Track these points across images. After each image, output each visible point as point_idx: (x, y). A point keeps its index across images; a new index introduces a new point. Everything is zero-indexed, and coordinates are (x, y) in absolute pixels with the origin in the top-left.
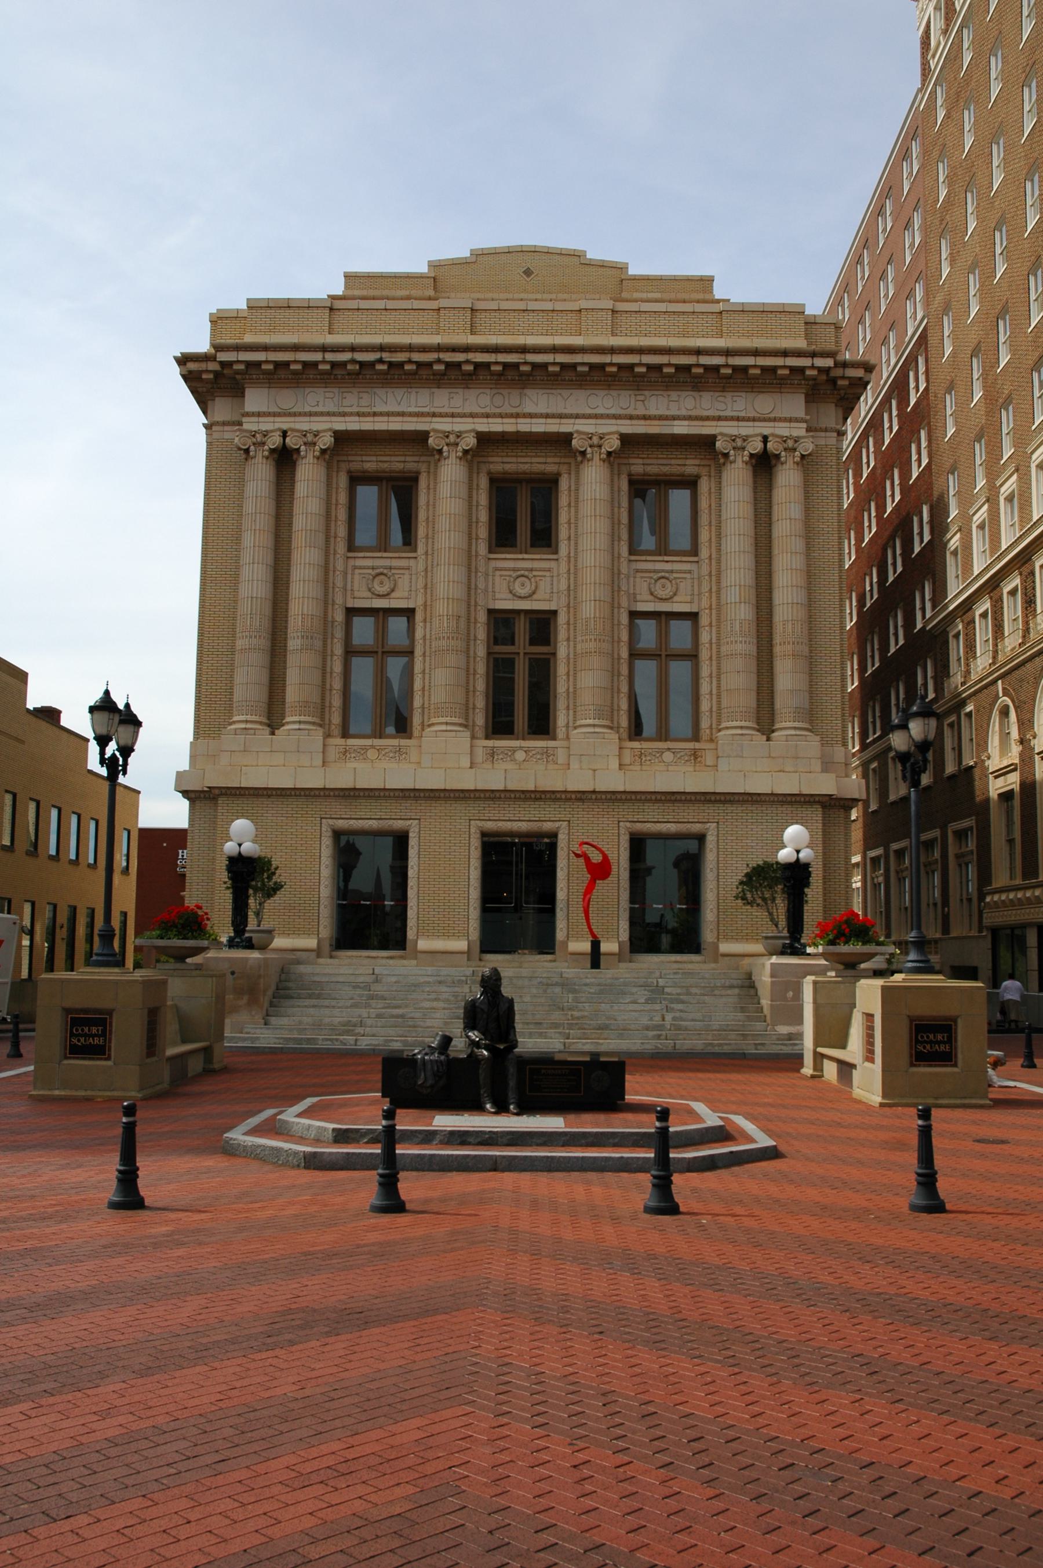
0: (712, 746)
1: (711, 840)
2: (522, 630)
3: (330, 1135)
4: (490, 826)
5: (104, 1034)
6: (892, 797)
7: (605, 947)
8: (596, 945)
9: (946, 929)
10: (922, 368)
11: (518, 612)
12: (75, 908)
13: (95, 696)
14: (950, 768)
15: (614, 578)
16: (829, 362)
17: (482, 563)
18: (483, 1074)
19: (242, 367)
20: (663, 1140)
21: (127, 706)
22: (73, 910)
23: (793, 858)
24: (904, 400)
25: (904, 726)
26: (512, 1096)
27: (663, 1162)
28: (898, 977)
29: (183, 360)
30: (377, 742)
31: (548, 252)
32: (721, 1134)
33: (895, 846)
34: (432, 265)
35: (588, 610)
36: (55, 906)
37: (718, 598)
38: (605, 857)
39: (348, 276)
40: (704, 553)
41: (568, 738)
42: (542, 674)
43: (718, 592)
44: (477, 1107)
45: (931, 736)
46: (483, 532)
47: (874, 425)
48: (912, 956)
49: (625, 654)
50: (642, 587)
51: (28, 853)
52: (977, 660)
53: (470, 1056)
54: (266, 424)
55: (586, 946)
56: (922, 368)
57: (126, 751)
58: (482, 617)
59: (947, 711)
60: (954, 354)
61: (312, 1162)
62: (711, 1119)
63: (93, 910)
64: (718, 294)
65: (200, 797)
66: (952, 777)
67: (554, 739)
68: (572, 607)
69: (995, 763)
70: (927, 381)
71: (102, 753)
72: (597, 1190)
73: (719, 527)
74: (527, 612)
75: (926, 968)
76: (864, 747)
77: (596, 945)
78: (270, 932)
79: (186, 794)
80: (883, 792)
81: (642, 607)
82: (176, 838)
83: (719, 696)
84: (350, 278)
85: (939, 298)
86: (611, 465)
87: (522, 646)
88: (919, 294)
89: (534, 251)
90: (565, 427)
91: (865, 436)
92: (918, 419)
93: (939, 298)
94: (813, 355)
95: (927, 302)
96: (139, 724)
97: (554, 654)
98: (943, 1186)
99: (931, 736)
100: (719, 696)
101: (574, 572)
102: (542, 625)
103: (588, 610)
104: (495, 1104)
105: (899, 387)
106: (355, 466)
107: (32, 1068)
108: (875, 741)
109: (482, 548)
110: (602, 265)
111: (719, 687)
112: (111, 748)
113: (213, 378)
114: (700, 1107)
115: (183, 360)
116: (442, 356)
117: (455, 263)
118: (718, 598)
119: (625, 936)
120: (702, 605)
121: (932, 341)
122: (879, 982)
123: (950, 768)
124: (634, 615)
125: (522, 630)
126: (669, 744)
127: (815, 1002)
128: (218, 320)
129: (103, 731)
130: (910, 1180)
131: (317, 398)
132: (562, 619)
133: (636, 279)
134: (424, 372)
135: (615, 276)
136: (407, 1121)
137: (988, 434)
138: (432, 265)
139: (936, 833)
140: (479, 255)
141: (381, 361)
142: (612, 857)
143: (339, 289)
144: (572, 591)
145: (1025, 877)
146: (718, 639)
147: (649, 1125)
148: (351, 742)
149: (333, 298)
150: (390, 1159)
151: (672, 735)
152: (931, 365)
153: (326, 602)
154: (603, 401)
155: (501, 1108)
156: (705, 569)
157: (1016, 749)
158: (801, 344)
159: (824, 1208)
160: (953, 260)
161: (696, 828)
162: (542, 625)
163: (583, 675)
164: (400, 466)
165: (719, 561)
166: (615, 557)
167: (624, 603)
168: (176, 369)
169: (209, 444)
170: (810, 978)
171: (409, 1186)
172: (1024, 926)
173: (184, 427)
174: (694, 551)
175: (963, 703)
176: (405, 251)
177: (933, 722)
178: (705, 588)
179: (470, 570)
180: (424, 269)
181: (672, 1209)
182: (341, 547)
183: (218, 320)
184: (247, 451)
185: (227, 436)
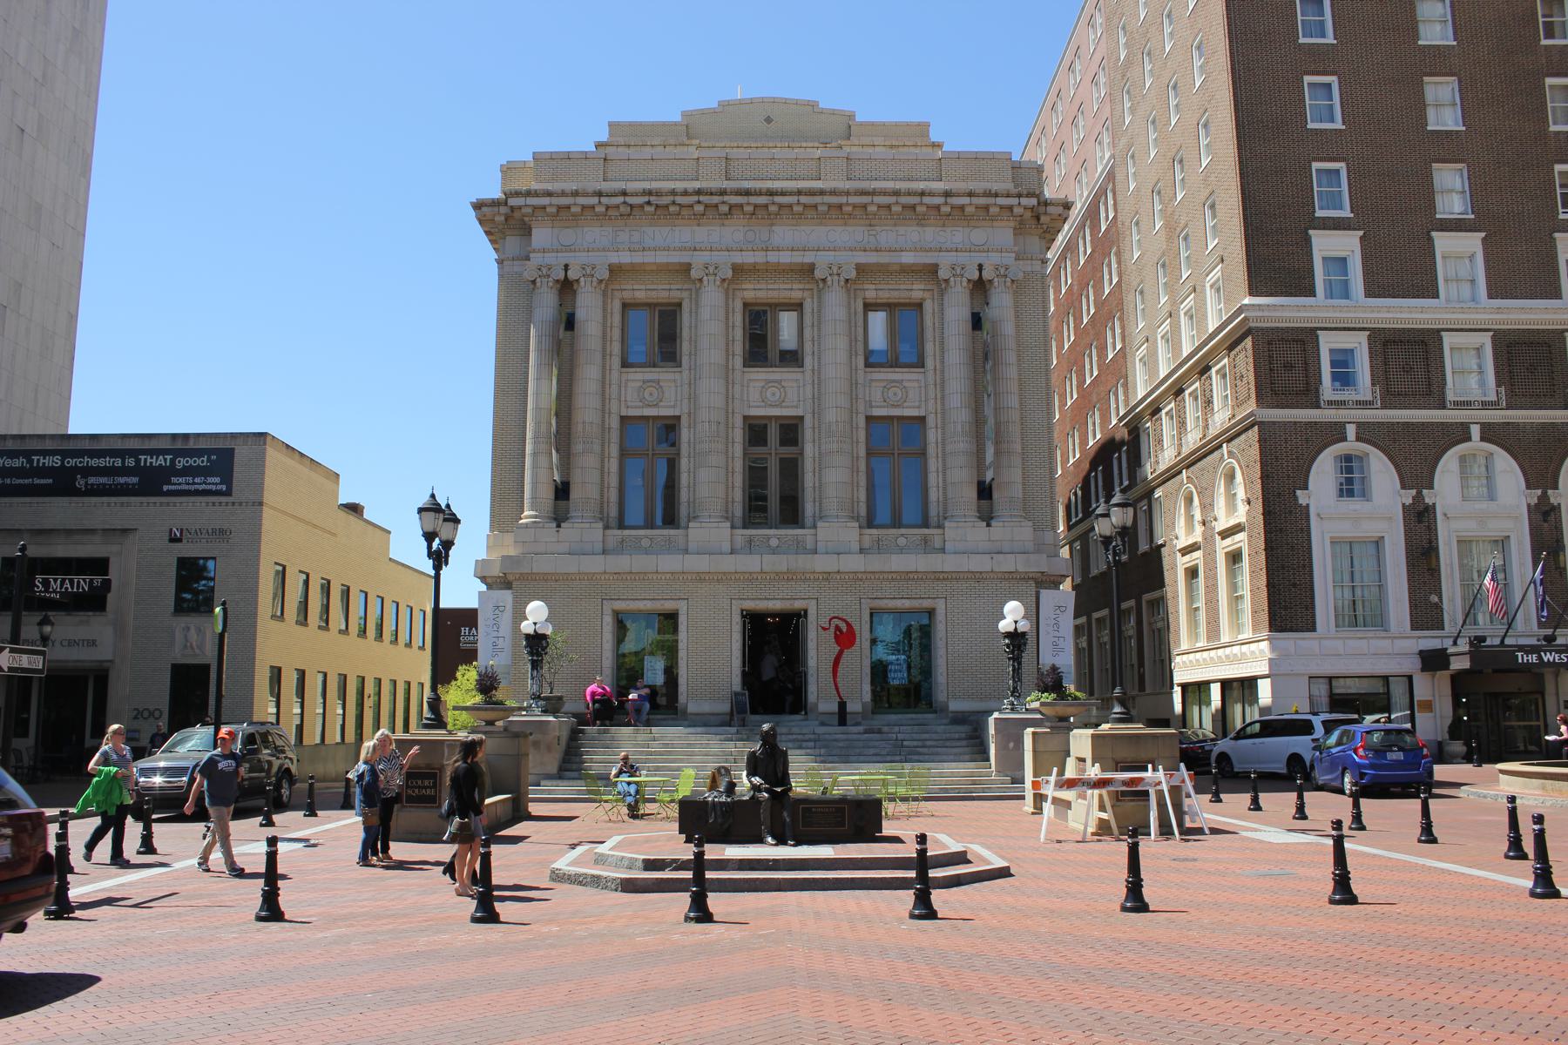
0: (939, 531)
1: (940, 616)
2: (773, 434)
3: (640, 864)
4: (750, 605)
5: (435, 786)
6: (1094, 572)
7: (850, 708)
8: (842, 705)
9: (1142, 687)
10: (1111, 202)
11: (770, 418)
12: (279, 669)
13: (423, 500)
14: (1143, 547)
15: (853, 384)
16: (1034, 201)
17: (738, 374)
18: (764, 814)
19: (529, 210)
20: (922, 862)
21: (448, 506)
22: (379, 682)
23: (1011, 629)
24: (1095, 226)
25: (1107, 515)
26: (788, 833)
27: (923, 877)
28: (1105, 726)
29: (478, 206)
30: (649, 532)
31: (786, 102)
32: (961, 858)
33: (1096, 615)
34: (684, 114)
35: (833, 415)
36: (325, 675)
37: (943, 404)
38: (848, 625)
39: (611, 125)
40: (929, 362)
41: (815, 527)
42: (791, 469)
43: (943, 398)
44: (759, 840)
45: (1129, 523)
46: (738, 348)
47: (1071, 247)
48: (1117, 709)
49: (862, 453)
50: (877, 395)
51: (340, 632)
52: (1163, 454)
53: (752, 798)
54: (550, 258)
55: (835, 708)
56: (1111, 202)
57: (448, 545)
58: (739, 422)
59: (1142, 498)
60: (1137, 189)
61: (629, 886)
62: (955, 847)
63: (422, 685)
64: (934, 138)
65: (497, 579)
66: (1145, 554)
67: (803, 527)
68: (817, 412)
69: (1183, 542)
70: (1116, 210)
71: (429, 547)
72: (866, 903)
73: (942, 343)
74: (777, 418)
75: (1127, 718)
76: (1070, 528)
77: (842, 705)
78: (560, 698)
79: (483, 579)
80: (1085, 568)
81: (877, 412)
82: (467, 617)
83: (945, 489)
84: (612, 126)
85: (1124, 141)
86: (848, 291)
87: (773, 450)
88: (1106, 140)
89: (774, 101)
90: (809, 258)
91: (1063, 257)
92: (1108, 244)
93: (1124, 141)
94: (1019, 196)
95: (1114, 145)
96: (457, 521)
97: (802, 454)
98: (1147, 893)
99: (1129, 523)
100: (945, 489)
101: (818, 382)
102: (791, 431)
103: (833, 415)
104: (774, 837)
105: (1092, 213)
106: (627, 295)
107: (488, 801)
108: (1077, 523)
109: (739, 361)
110: (833, 113)
111: (944, 481)
112: (436, 544)
113: (505, 219)
114: (943, 838)
115: (478, 206)
116: (702, 198)
117: (703, 112)
118: (943, 404)
119: (867, 697)
120: (928, 409)
121: (1119, 177)
122: (1091, 731)
123: (1143, 547)
124: (869, 419)
125: (773, 434)
126: (903, 531)
127: (1034, 751)
128: (508, 170)
129: (430, 529)
130: (1123, 891)
131: (594, 234)
132: (808, 422)
133: (862, 124)
134: (685, 212)
135: (847, 127)
136: (713, 852)
137: (1168, 264)
138: (684, 114)
139: (1132, 603)
140: (725, 105)
141: (649, 203)
142: (856, 628)
143: (604, 136)
144: (817, 399)
145: (1209, 639)
146: (944, 440)
147: (909, 850)
148: (626, 532)
149: (599, 145)
150: (699, 879)
151: (904, 522)
152: (1119, 198)
153: (603, 411)
154: (840, 234)
155: (781, 841)
156: (930, 374)
157: (1199, 529)
158: (1010, 186)
159: (1052, 912)
160: (1132, 110)
161: (926, 604)
162: (791, 431)
163: (832, 473)
164: (665, 294)
165: (943, 372)
166: (853, 370)
167: (861, 408)
168: (472, 213)
169: (501, 276)
170: (1030, 730)
171: (715, 901)
172: (1208, 683)
173: (480, 261)
174: (920, 364)
175: (1152, 491)
176: (663, 105)
177: (1130, 510)
178: (931, 394)
179: (728, 382)
180: (678, 118)
181: (931, 914)
182: (616, 361)
183: (508, 170)
184: (534, 282)
185: (516, 269)
